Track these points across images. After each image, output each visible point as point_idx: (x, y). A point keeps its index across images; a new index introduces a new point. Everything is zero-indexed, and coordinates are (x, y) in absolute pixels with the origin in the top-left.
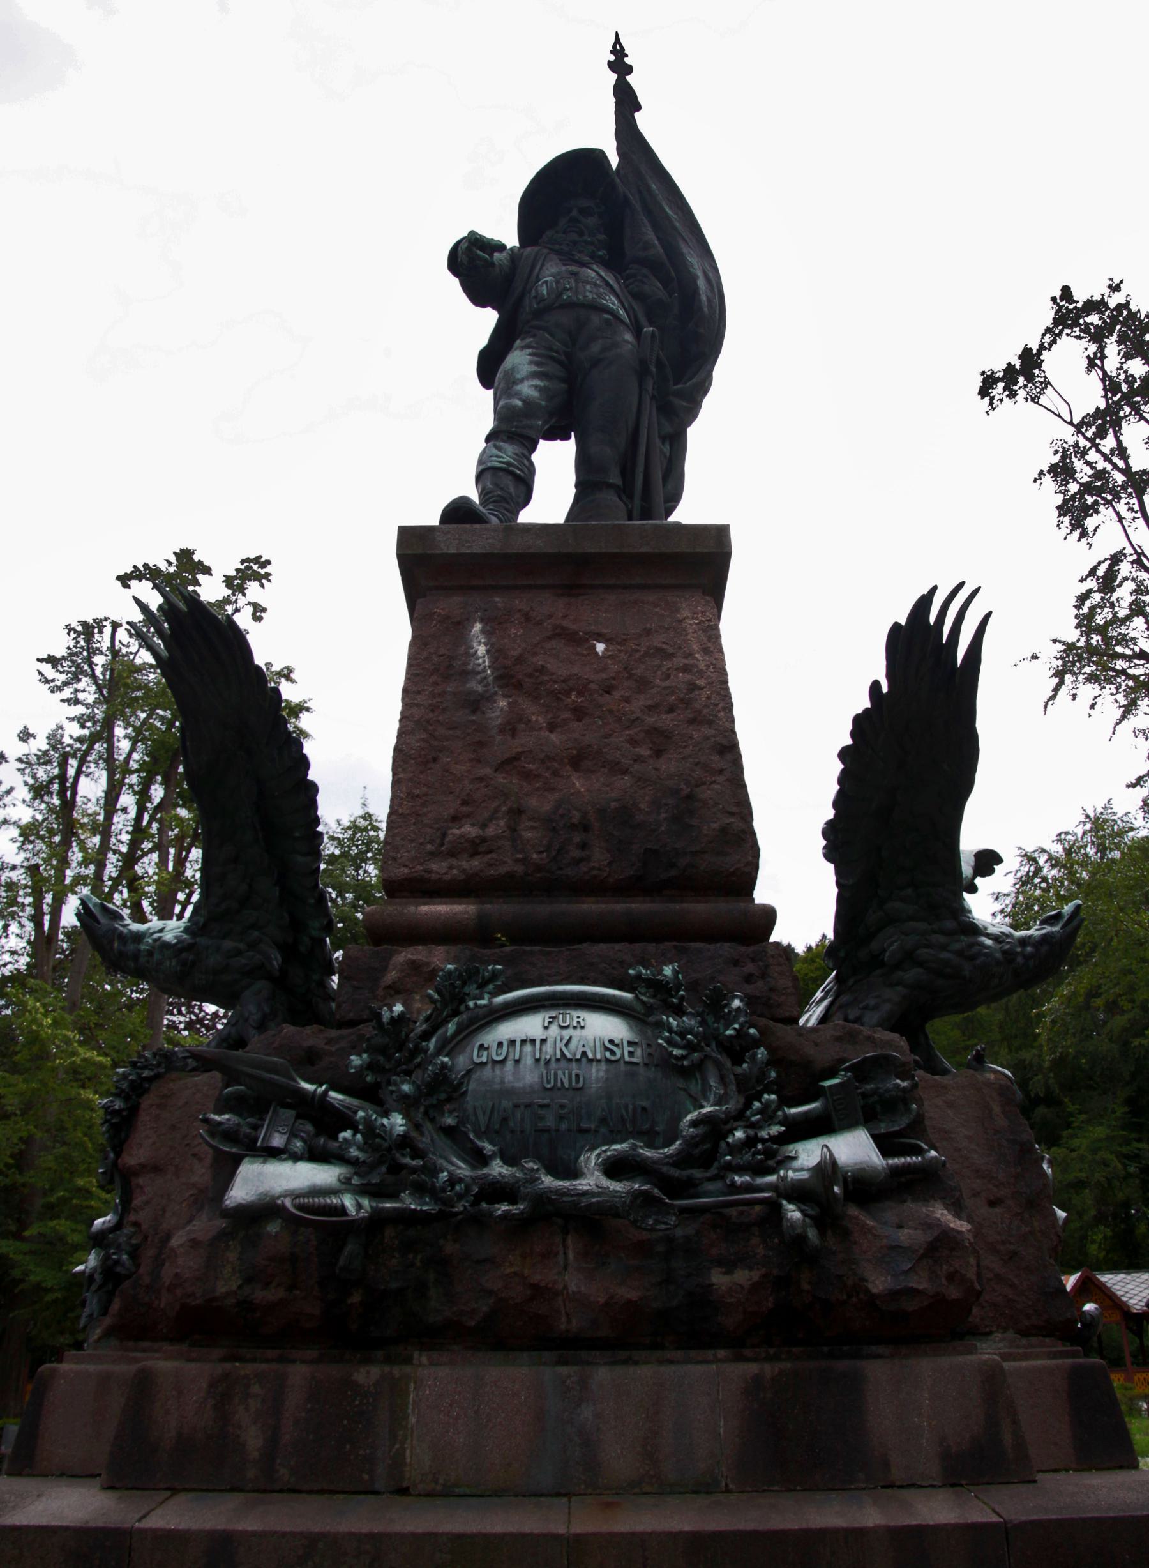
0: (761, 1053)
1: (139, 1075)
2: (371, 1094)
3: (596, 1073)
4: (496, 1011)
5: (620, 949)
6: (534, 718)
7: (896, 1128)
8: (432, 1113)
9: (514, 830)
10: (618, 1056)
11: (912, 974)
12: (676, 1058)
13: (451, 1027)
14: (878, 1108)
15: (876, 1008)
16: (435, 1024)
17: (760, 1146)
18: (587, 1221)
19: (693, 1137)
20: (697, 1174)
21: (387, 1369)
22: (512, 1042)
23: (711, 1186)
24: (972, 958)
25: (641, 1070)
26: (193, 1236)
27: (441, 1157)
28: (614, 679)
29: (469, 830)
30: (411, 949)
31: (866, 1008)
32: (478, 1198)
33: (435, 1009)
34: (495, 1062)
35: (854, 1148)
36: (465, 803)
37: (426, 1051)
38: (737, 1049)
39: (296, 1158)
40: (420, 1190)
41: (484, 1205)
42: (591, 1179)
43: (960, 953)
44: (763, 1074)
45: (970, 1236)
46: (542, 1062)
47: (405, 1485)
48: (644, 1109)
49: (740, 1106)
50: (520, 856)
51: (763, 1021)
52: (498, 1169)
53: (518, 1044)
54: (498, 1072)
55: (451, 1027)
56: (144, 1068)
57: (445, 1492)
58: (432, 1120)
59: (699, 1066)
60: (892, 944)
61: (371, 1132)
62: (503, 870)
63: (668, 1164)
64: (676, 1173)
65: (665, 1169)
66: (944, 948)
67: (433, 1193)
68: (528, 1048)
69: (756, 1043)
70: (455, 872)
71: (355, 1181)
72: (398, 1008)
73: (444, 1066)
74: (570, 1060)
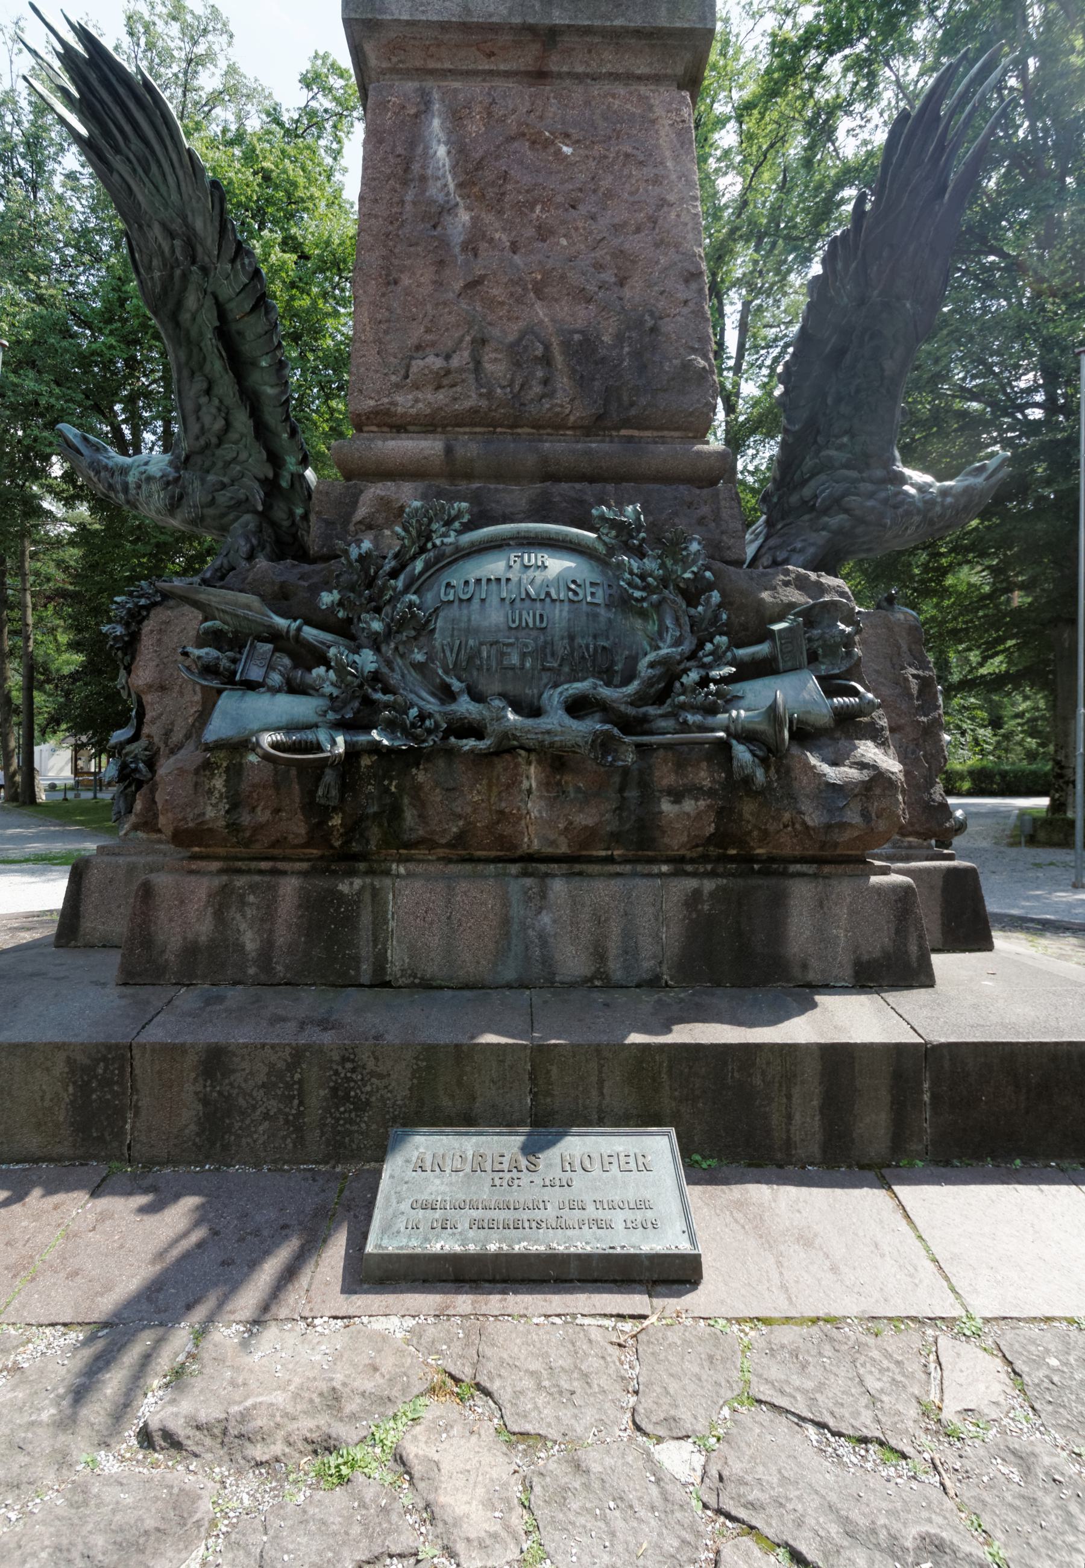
0: (716, 597)
1: (136, 604)
2: (345, 630)
3: (559, 615)
4: (463, 549)
5: (588, 490)
6: (497, 236)
7: (837, 671)
8: (401, 649)
9: (478, 363)
10: (581, 597)
11: (836, 520)
12: (636, 600)
13: (419, 565)
14: (820, 651)
15: (802, 551)
16: (402, 562)
17: (712, 686)
18: (557, 760)
19: (650, 678)
20: (652, 710)
21: (368, 880)
22: (478, 581)
23: (663, 724)
24: (895, 507)
25: (602, 611)
26: (180, 765)
27: (411, 691)
28: (581, 190)
29: (436, 363)
30: (380, 485)
31: (794, 550)
32: (450, 731)
33: (403, 546)
34: (461, 600)
35: (798, 693)
36: (428, 331)
37: (394, 589)
38: (692, 594)
39: (275, 691)
40: (390, 727)
41: (453, 739)
42: (556, 722)
43: (885, 501)
44: (716, 617)
45: (901, 776)
46: (507, 602)
47: (388, 978)
48: (604, 648)
49: (693, 647)
50: (484, 390)
51: (718, 565)
52: (465, 706)
53: (484, 582)
54: (465, 612)
55: (419, 565)
56: (140, 597)
57: (506, 519)
58: (402, 656)
59: (658, 606)
60: (823, 491)
61: (341, 670)
62: (468, 404)
63: (626, 703)
64: (631, 711)
65: (622, 708)
66: (871, 495)
67: (407, 733)
68: (494, 586)
69: (710, 587)
70: (420, 405)
71: (331, 716)
72: (367, 545)
73: (411, 605)
74: (534, 600)
